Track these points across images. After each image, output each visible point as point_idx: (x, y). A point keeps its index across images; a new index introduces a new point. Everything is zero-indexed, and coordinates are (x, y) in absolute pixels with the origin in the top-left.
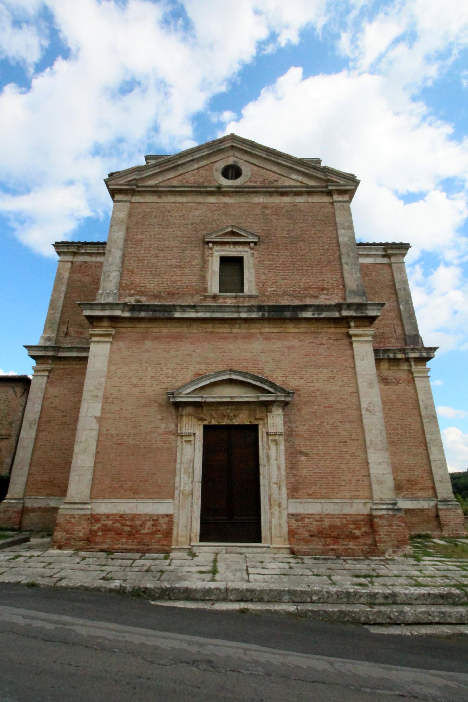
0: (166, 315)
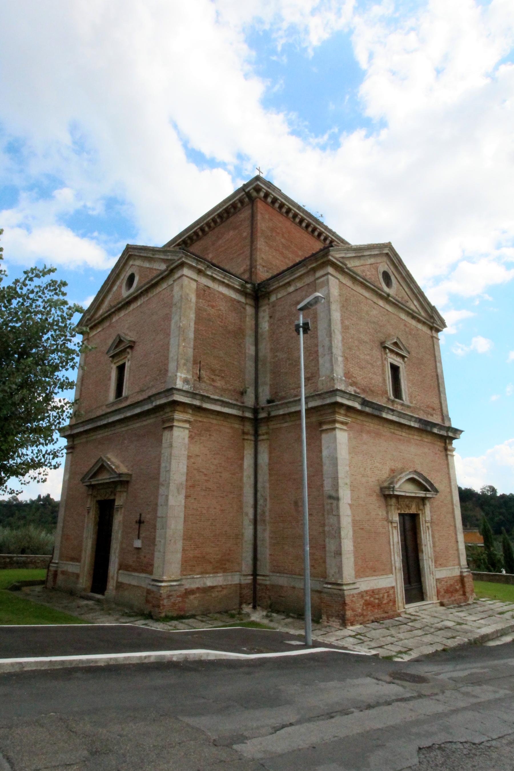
0: (376, 413)
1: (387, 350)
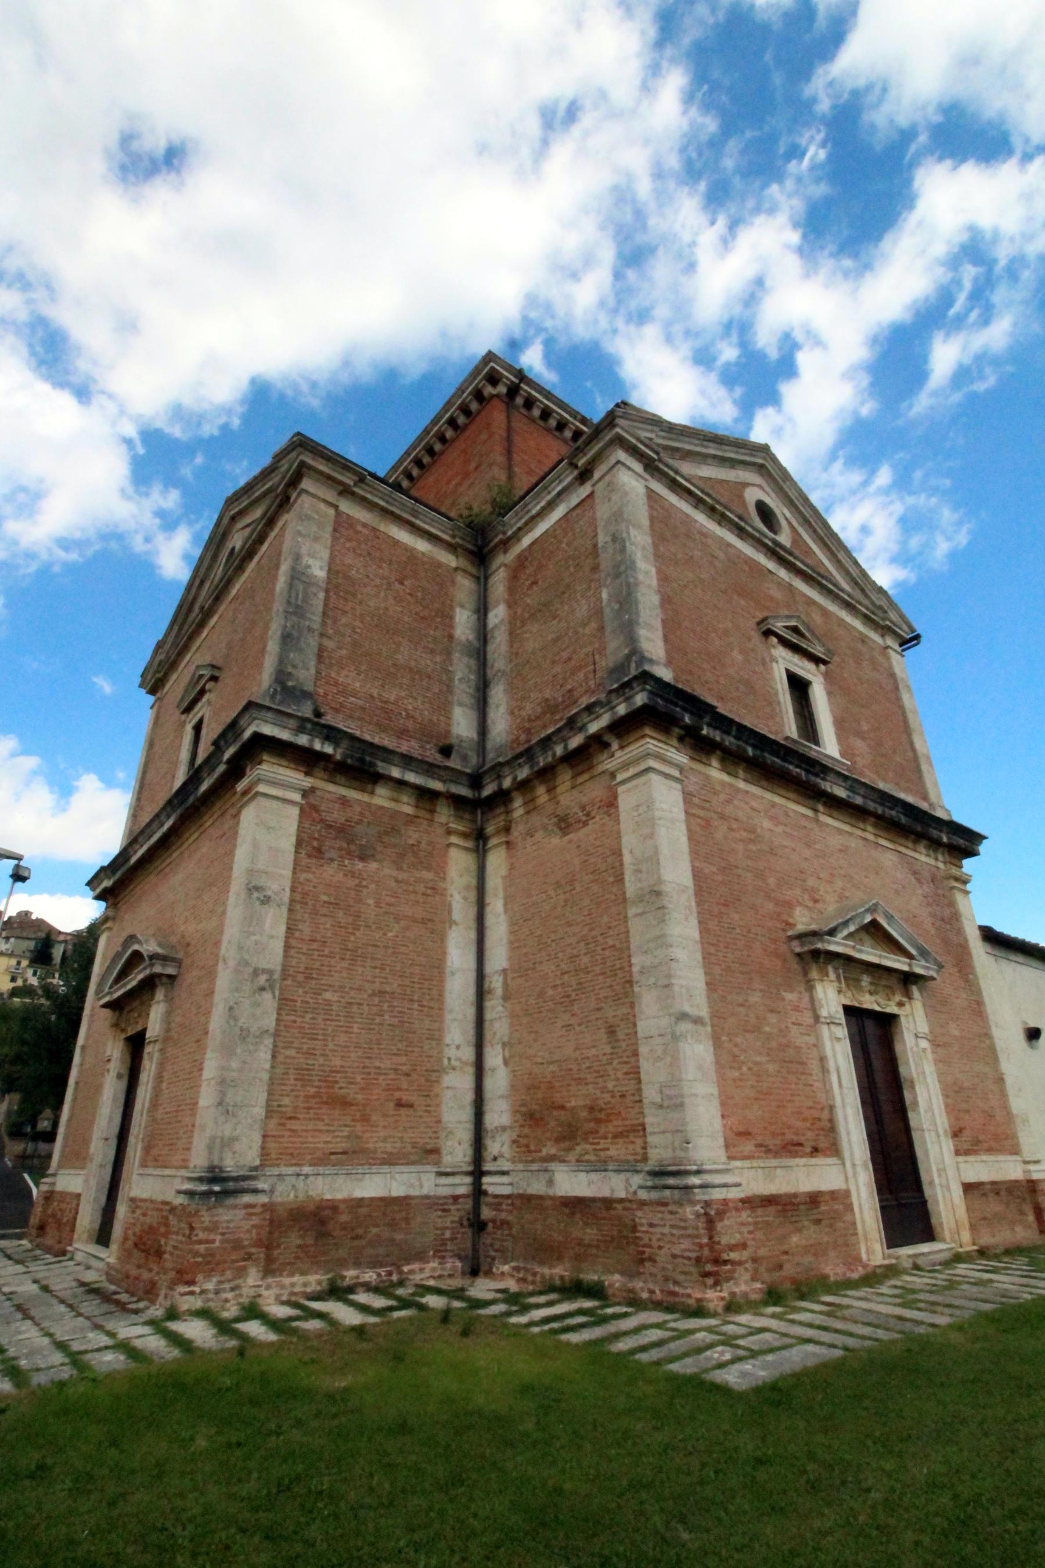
1: (775, 640)
